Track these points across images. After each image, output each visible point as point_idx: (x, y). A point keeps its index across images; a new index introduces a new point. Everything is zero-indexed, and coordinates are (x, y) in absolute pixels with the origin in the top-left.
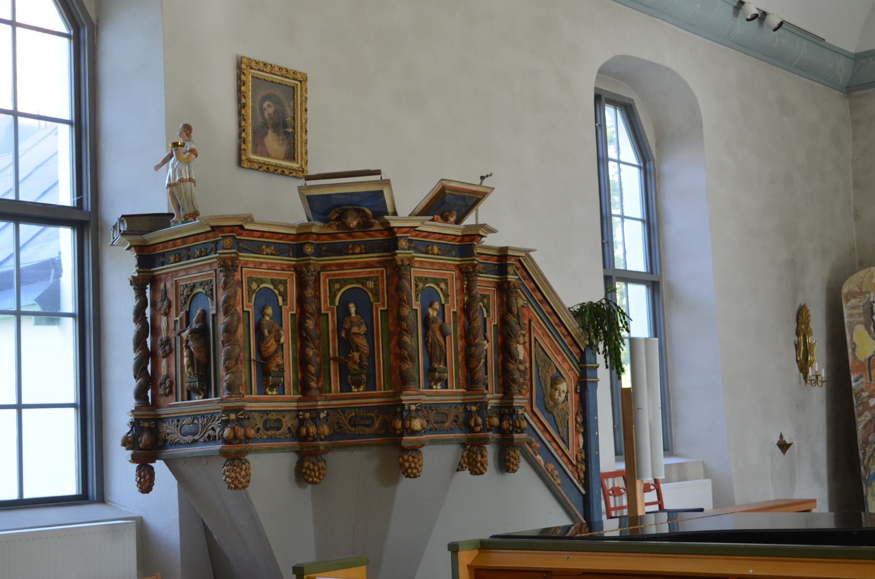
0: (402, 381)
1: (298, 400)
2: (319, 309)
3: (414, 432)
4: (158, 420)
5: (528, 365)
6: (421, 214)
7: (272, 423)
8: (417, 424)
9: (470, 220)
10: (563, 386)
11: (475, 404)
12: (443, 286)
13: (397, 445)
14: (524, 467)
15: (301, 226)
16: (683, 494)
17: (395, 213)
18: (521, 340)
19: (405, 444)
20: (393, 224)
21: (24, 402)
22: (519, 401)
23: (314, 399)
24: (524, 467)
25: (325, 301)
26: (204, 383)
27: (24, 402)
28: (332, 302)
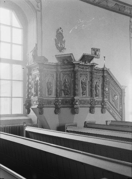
0: (75, 95)
1: (55, 98)
2: (60, 80)
3: (76, 105)
4: (30, 101)
5: (108, 92)
6: (80, 61)
7: (49, 102)
8: (77, 103)
9: (92, 62)
10: (116, 97)
11: (92, 99)
12: (86, 75)
13: (73, 107)
14: (107, 112)
15: (57, 63)
16: (126, 120)
17: (75, 60)
18: (107, 87)
19: (75, 107)
20: (74, 63)
21: (13, 96)
22: (106, 99)
23: (58, 98)
24: (107, 112)
25: (62, 78)
26: (36, 95)
27: (13, 96)
28: (63, 78)
